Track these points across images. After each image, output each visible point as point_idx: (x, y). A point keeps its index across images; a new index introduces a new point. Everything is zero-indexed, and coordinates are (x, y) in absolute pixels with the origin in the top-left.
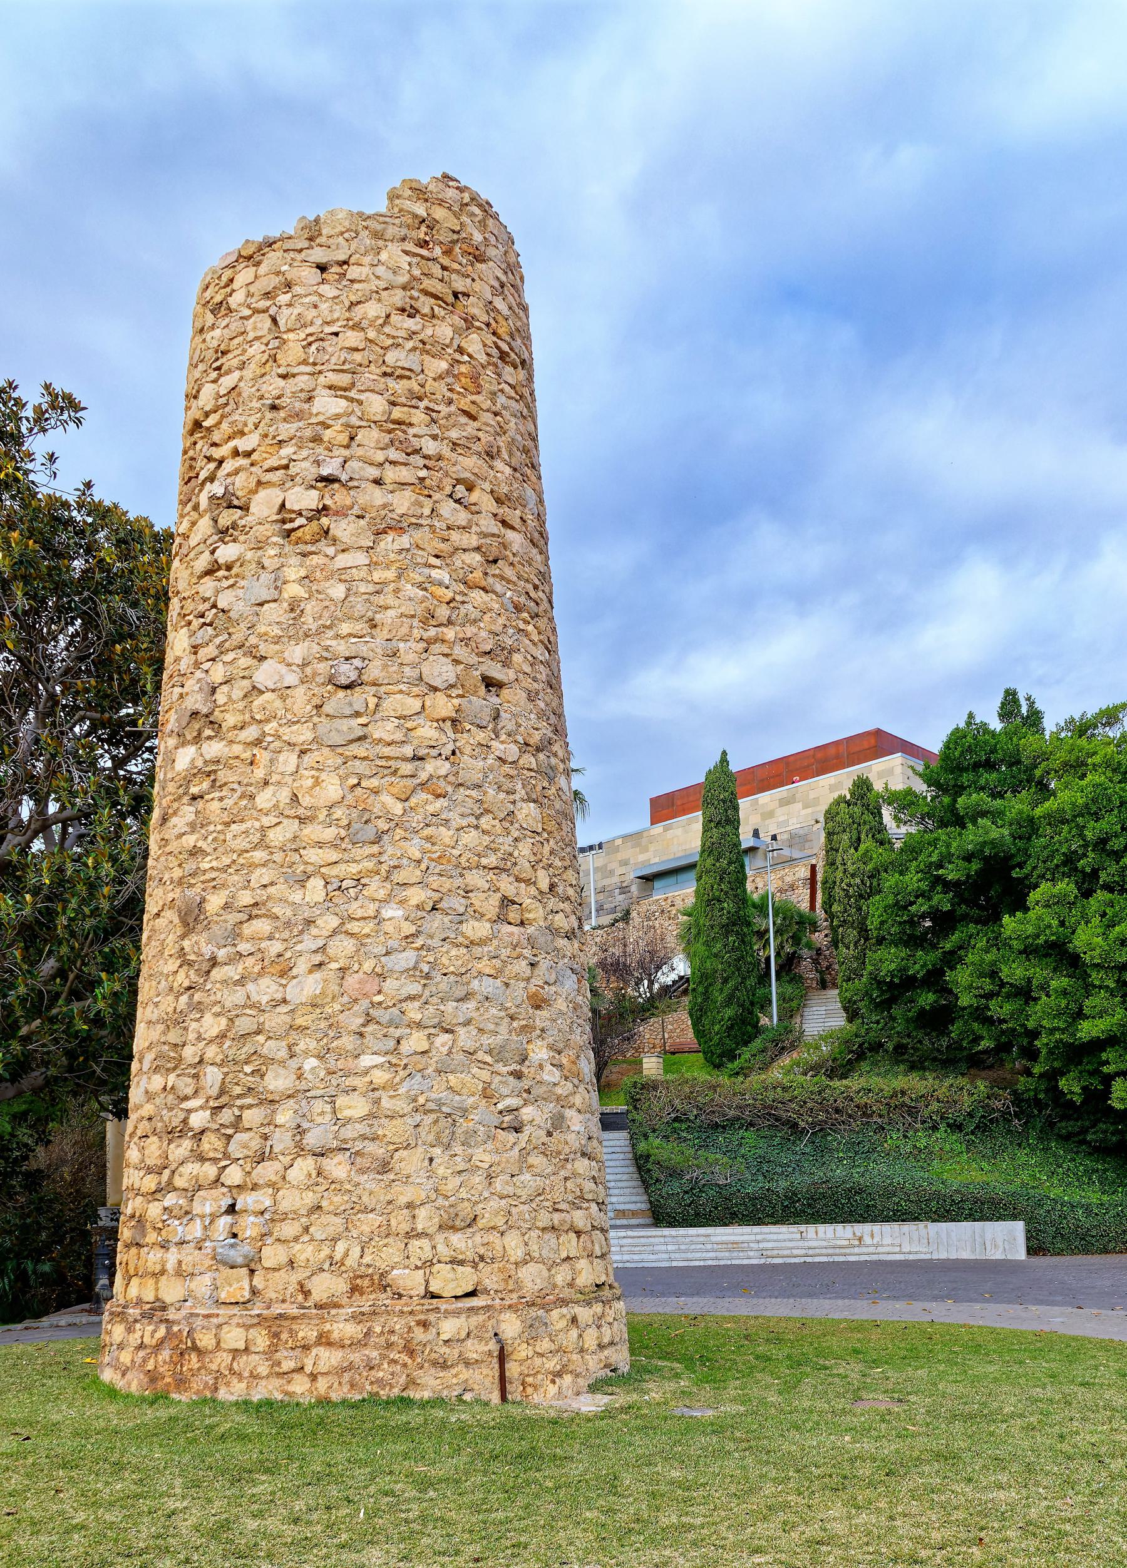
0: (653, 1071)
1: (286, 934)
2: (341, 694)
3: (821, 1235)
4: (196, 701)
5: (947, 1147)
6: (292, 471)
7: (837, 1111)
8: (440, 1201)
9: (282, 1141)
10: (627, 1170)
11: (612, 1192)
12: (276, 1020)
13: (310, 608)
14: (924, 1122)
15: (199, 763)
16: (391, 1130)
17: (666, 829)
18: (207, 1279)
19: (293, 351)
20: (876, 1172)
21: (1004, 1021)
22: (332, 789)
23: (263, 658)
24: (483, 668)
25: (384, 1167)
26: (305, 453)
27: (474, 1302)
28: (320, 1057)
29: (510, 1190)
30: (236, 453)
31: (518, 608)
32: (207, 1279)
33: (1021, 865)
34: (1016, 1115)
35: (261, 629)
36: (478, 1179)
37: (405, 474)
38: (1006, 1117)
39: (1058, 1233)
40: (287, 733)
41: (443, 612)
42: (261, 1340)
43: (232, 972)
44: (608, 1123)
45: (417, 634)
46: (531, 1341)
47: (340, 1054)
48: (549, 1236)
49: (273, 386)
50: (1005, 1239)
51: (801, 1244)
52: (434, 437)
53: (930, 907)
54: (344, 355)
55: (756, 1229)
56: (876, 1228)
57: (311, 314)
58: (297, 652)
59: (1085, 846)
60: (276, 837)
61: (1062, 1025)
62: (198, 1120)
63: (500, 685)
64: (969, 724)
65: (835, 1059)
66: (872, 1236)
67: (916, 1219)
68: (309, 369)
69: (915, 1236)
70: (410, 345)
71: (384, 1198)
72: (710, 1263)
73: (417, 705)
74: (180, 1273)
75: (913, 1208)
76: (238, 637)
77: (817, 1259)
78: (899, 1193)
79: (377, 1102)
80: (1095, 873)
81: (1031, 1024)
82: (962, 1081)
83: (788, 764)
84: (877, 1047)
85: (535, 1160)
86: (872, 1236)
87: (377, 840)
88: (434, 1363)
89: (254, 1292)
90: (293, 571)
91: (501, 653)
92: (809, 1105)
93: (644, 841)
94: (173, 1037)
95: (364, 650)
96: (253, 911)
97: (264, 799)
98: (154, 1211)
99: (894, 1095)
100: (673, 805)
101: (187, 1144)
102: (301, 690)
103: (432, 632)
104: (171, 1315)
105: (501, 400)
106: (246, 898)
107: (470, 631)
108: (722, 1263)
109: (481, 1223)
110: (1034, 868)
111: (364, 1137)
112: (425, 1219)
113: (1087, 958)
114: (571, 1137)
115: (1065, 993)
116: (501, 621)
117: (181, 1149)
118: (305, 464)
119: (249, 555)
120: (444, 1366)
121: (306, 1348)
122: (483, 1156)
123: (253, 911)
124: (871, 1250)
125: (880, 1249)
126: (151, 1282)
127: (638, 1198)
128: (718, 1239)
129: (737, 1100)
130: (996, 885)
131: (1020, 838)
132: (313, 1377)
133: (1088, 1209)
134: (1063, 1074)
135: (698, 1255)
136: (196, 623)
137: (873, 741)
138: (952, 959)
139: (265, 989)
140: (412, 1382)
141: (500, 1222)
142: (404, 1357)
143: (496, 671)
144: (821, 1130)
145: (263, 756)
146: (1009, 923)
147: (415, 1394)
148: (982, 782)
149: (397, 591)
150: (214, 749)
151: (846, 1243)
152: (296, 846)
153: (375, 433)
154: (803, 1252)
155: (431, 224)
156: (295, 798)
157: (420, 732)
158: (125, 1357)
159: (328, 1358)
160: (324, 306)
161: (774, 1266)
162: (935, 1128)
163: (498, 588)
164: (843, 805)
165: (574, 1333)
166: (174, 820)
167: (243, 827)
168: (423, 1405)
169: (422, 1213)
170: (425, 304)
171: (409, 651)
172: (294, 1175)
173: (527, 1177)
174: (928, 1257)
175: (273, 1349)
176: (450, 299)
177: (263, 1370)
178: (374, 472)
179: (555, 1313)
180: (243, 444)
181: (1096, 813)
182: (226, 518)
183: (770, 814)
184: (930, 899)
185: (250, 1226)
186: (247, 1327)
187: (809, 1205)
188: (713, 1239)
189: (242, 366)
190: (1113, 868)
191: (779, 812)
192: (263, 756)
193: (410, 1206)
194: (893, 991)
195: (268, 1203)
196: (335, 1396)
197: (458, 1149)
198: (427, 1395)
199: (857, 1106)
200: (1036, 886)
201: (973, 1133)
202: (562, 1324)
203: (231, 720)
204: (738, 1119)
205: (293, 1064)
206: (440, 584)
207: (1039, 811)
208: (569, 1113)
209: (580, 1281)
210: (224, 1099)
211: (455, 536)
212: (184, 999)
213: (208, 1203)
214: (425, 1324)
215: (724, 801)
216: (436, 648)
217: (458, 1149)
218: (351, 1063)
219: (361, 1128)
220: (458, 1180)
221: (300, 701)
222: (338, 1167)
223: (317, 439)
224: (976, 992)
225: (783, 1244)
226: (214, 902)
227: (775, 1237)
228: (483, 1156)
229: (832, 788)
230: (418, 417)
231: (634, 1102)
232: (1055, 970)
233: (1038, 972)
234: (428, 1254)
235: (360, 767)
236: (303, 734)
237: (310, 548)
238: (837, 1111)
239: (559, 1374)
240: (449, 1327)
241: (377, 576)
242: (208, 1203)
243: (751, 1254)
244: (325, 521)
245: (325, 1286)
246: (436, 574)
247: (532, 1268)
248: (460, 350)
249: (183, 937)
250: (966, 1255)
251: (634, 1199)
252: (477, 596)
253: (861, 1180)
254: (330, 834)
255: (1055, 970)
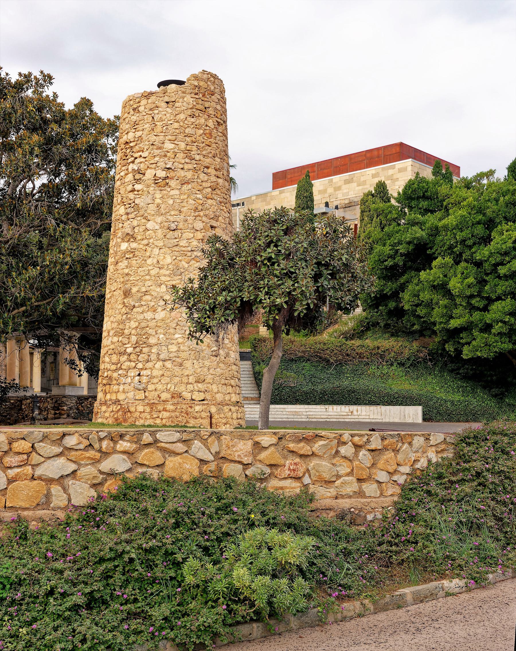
0: (264, 333)
1: (155, 300)
2: (171, 232)
3: (335, 410)
4: (129, 230)
5: (397, 374)
6: (158, 165)
7: (348, 355)
8: (196, 375)
9: (153, 357)
10: (250, 379)
11: (242, 389)
12: (152, 324)
13: (163, 206)
14: (387, 362)
15: (129, 249)
16: (183, 355)
17: (281, 193)
18: (132, 393)
19: (159, 129)
20: (363, 383)
21: (422, 317)
22: (169, 260)
23: (149, 220)
24: (211, 223)
25: (181, 365)
26: (162, 160)
27: (204, 402)
28: (164, 335)
29: (214, 373)
30: (141, 156)
31: (221, 203)
32: (132, 393)
33: (431, 248)
34: (430, 360)
35: (149, 212)
36: (206, 369)
37: (190, 166)
38: (425, 360)
39: (438, 413)
40: (156, 243)
41: (200, 207)
42: (148, 409)
43: (140, 310)
44: (243, 356)
45: (193, 214)
46: (219, 414)
47: (170, 334)
48: (224, 386)
49: (153, 138)
50: (414, 414)
51: (325, 413)
52: (198, 154)
53: (394, 263)
54: (174, 130)
55: (306, 406)
56: (359, 407)
57: (164, 117)
58: (159, 219)
59: (457, 242)
60: (153, 272)
61: (444, 321)
62: (129, 350)
63: (215, 227)
64: (417, 177)
65: (354, 330)
66: (357, 411)
67: (378, 404)
68: (163, 134)
69: (376, 412)
70: (192, 126)
71: (181, 373)
72: (284, 420)
73: (192, 235)
74: (124, 392)
75: (377, 400)
76: (141, 213)
77: (331, 420)
78: (371, 393)
79: (179, 347)
80: (461, 254)
81: (432, 320)
82: (407, 344)
83: (351, 159)
84: (376, 324)
85: (221, 365)
86: (357, 411)
87: (181, 275)
88: (193, 417)
89: (145, 397)
90: (158, 195)
91: (216, 218)
92: (335, 352)
93: (268, 198)
94: (121, 326)
95: (178, 220)
96: (146, 293)
97: (149, 261)
98: (115, 375)
99: (374, 349)
100: (286, 178)
101: (126, 357)
102: (160, 230)
103: (197, 214)
104: (122, 403)
105: (218, 138)
106: (144, 289)
107: (207, 212)
108: (290, 420)
109: (206, 381)
110: (437, 250)
111: (175, 357)
112: (192, 379)
113: (453, 292)
114: (231, 359)
115: (446, 307)
116: (216, 208)
117: (124, 358)
118: (162, 163)
119: (145, 189)
120: (196, 418)
121: (160, 412)
122: (207, 363)
123: (146, 293)
124: (356, 417)
125: (360, 417)
126: (114, 394)
127: (254, 392)
128: (289, 410)
129: (303, 348)
130: (421, 255)
131: (432, 235)
132: (162, 419)
133: (452, 402)
134: (447, 342)
135: (280, 416)
136: (127, 206)
137: (398, 149)
138: (403, 288)
139: (149, 315)
140: (187, 422)
141: (211, 381)
142: (185, 415)
143: (214, 224)
144: (340, 364)
145: (149, 249)
146: (423, 275)
147: (189, 425)
148: (421, 206)
149: (187, 202)
150: (134, 245)
151: (345, 414)
152: (158, 276)
153: (182, 154)
154: (326, 417)
155: (199, 87)
156: (158, 262)
157: (193, 243)
158: (107, 415)
159: (166, 414)
160: (168, 115)
161: (312, 422)
162: (392, 365)
163: (215, 198)
164: (370, 196)
165: (230, 413)
166: (120, 264)
167: (143, 269)
168: (190, 427)
169: (191, 378)
170: (197, 113)
171: (190, 219)
172: (156, 366)
173: (218, 369)
174: (381, 421)
175: (151, 412)
176: (204, 110)
177: (148, 417)
178: (181, 166)
179: (225, 407)
180: (144, 155)
181: (461, 228)
182: (138, 176)
183: (339, 188)
184: (394, 259)
185: (144, 379)
186: (144, 406)
187: (331, 397)
188: (287, 410)
189: (143, 130)
190: (468, 253)
191: (344, 187)
192: (149, 249)
193: (188, 376)
194: (377, 301)
195: (150, 373)
196: (167, 424)
197: (201, 361)
198: (191, 425)
199: (357, 354)
200: (436, 258)
201: (409, 367)
202: (227, 410)
203: (139, 237)
204: (303, 357)
205: (157, 336)
206: (199, 199)
207: (440, 224)
208: (231, 352)
209: (232, 400)
210: (137, 345)
211: (204, 184)
212: (125, 316)
213: (132, 373)
214: (191, 407)
215: (306, 197)
216: (198, 218)
217: (201, 361)
218: (172, 337)
219: (175, 354)
220: (200, 369)
221: (160, 234)
222: (168, 364)
223: (165, 156)
224: (410, 303)
225: (317, 413)
226: (134, 290)
227: (314, 410)
228: (207, 363)
229: (374, 176)
230: (194, 148)
231: (255, 347)
232: (443, 296)
233: (436, 297)
234: (192, 389)
235: (176, 254)
236: (160, 244)
237: (163, 188)
238: (348, 355)
239: (226, 424)
240: (197, 408)
241: (182, 197)
242: (132, 373)
243: (303, 417)
244: (167, 181)
245: (165, 396)
246: (198, 196)
247: (219, 395)
248: (207, 126)
249: (124, 299)
250: (397, 420)
251: (252, 392)
252: (210, 201)
253: (355, 387)
254: (168, 272)
255: (443, 296)
